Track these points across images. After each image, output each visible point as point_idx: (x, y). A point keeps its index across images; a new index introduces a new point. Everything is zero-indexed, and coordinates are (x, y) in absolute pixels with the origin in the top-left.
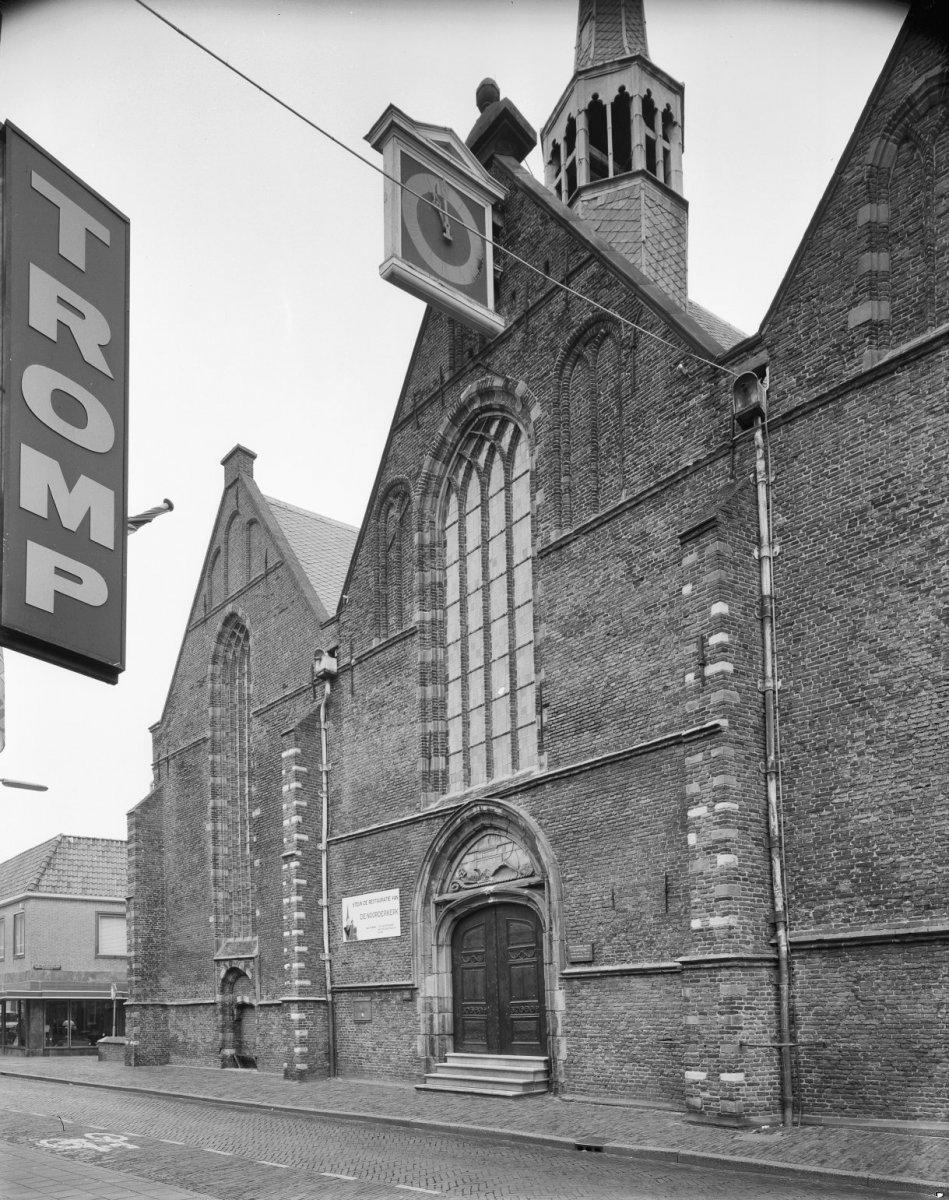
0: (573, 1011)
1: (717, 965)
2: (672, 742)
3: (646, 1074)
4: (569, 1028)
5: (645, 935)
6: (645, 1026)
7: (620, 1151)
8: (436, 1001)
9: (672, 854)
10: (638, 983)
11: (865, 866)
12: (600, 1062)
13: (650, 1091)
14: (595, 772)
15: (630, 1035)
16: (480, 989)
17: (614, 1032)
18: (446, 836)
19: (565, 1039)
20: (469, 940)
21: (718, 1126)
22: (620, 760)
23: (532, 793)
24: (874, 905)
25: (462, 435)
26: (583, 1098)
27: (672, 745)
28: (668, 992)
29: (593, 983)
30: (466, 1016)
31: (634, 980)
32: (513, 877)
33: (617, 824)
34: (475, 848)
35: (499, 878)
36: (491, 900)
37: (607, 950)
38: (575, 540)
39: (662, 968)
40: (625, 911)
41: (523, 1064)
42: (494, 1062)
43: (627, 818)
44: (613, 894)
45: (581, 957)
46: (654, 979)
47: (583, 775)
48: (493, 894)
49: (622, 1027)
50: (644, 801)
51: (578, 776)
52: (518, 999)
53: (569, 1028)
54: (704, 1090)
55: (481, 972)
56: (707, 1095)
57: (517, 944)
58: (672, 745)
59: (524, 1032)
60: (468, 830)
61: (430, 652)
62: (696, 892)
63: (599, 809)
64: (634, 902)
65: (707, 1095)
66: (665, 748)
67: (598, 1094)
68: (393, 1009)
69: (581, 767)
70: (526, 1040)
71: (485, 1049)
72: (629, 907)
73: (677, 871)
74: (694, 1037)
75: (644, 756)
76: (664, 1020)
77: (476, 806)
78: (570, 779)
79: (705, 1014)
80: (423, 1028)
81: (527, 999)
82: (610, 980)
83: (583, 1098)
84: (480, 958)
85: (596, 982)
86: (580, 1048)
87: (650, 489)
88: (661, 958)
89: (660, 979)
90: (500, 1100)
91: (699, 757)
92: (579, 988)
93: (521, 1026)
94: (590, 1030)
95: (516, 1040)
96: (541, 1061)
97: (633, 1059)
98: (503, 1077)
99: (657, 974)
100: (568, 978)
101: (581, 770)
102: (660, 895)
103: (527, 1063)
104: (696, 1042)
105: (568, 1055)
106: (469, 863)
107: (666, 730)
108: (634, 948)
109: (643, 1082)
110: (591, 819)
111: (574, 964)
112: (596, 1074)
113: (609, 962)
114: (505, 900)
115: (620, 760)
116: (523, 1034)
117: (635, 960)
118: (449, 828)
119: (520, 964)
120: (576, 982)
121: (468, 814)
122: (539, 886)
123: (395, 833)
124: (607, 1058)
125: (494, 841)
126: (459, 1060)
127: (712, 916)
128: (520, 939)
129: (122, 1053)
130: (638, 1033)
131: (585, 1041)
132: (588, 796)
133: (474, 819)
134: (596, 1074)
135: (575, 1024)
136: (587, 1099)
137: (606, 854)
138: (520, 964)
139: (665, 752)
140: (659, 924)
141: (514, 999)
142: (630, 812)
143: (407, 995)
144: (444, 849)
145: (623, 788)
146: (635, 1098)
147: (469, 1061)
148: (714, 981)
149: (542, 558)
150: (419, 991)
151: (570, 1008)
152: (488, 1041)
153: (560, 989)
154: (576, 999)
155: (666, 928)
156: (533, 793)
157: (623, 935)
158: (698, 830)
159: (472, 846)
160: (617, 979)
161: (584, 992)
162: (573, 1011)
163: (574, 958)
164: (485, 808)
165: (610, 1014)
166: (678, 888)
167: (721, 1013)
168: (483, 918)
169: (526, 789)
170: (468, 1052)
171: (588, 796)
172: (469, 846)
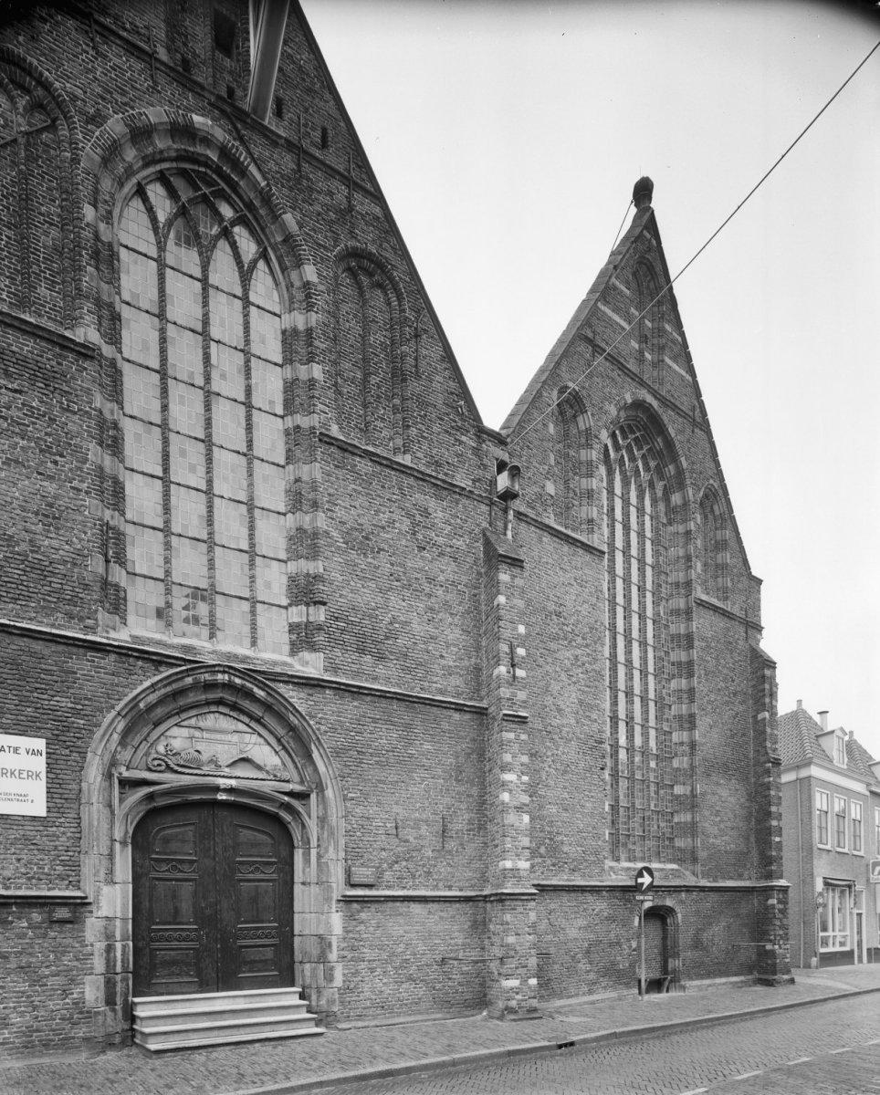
0: (351, 935)
1: (529, 897)
2: (453, 706)
3: (421, 991)
4: (345, 953)
5: (424, 866)
6: (421, 948)
7: (585, 1041)
8: (118, 923)
9: (447, 800)
10: (416, 908)
11: (551, 839)
12: (377, 985)
13: (423, 1006)
14: (384, 701)
15: (408, 957)
16: (186, 906)
17: (393, 954)
18: (163, 691)
19: (341, 964)
20: (166, 841)
21: (531, 1019)
22: (407, 701)
23: (307, 690)
24: (554, 865)
25: (177, 159)
26: (360, 1024)
27: (452, 709)
28: (441, 918)
29: (374, 907)
30: (156, 945)
31: (412, 905)
32: (261, 776)
33: (401, 758)
34: (193, 721)
35: (238, 772)
36: (222, 797)
37: (388, 875)
38: (360, 456)
39: (440, 897)
40: (407, 841)
41: (270, 998)
42: (226, 1001)
43: (411, 756)
44: (397, 823)
45: (365, 881)
46: (430, 905)
47: (369, 698)
48: (231, 790)
49: (400, 950)
50: (427, 746)
51: (363, 697)
52: (246, 922)
53: (345, 953)
54: (517, 993)
55: (187, 888)
56: (519, 997)
57: (251, 856)
58: (452, 709)
59: (255, 961)
60: (192, 698)
61: (682, 626)
62: (509, 839)
63: (386, 737)
64: (415, 835)
65: (519, 997)
66: (445, 708)
67: (375, 1017)
68: (22, 936)
69: (371, 689)
70: (259, 971)
71: (201, 986)
72: (411, 839)
73: (451, 815)
74: (512, 953)
75: (428, 707)
76: (436, 942)
77: (224, 672)
78: (356, 696)
79: (519, 935)
80: (99, 964)
81: (262, 922)
82: (390, 904)
83: (360, 1024)
84: (186, 867)
85: (376, 906)
86: (356, 973)
87: (436, 478)
88: (436, 887)
89: (435, 906)
90: (305, 1039)
91: (511, 736)
92: (359, 912)
93: (253, 955)
94: (368, 953)
95: (244, 972)
96: (295, 992)
97: (410, 979)
98: (248, 1017)
99: (433, 901)
100: (347, 901)
101: (371, 693)
102: (437, 833)
103: (279, 997)
104: (513, 957)
105: (344, 981)
106: (178, 738)
107: (441, 692)
108: (414, 877)
109: (419, 999)
110: (377, 744)
111: (354, 886)
112: (374, 997)
113: (389, 887)
114: (245, 800)
115: (407, 701)
116: (252, 965)
117: (415, 887)
118: (170, 684)
119: (254, 880)
120: (355, 906)
121: (207, 677)
122: (303, 796)
123: (38, 646)
124: (385, 981)
125: (225, 723)
126: (247, 1000)
127: (520, 859)
128: (254, 851)
129: (313, 1023)
130: (416, 955)
131: (363, 965)
132: (375, 721)
133: (210, 686)
134: (374, 997)
135: (353, 949)
136: (366, 1024)
137: (391, 783)
138: (254, 880)
139: (444, 711)
140: (436, 858)
141: (242, 923)
142: (414, 752)
143: (62, 913)
144: (151, 708)
145: (408, 727)
146: (410, 1015)
147: (179, 1005)
148: (525, 909)
149: (320, 440)
150: (93, 908)
151: (348, 932)
152: (198, 975)
153: (337, 911)
154: (354, 923)
155: (441, 862)
156: (311, 692)
157: (404, 863)
158: (510, 792)
159: (190, 718)
160: (398, 904)
161: (363, 916)
162: (351, 935)
163: (355, 880)
164: (238, 681)
165: (390, 937)
166: (452, 830)
167: (529, 934)
168: (193, 816)
169: (303, 684)
170: (162, 994)
171: (375, 721)
172: (184, 716)
